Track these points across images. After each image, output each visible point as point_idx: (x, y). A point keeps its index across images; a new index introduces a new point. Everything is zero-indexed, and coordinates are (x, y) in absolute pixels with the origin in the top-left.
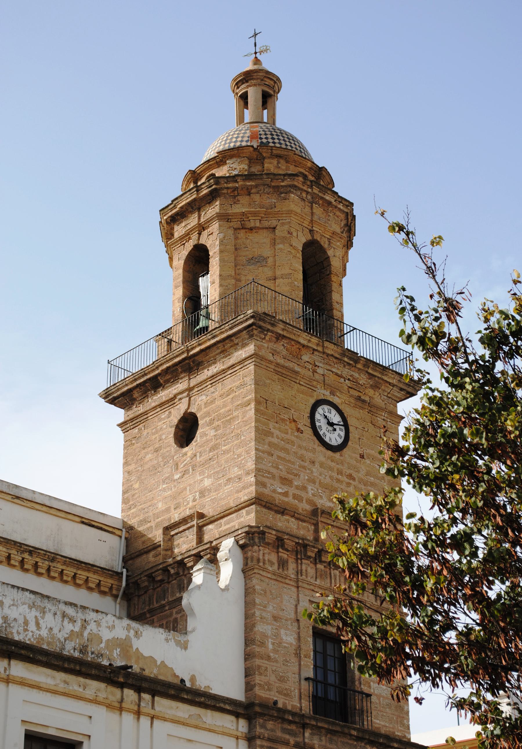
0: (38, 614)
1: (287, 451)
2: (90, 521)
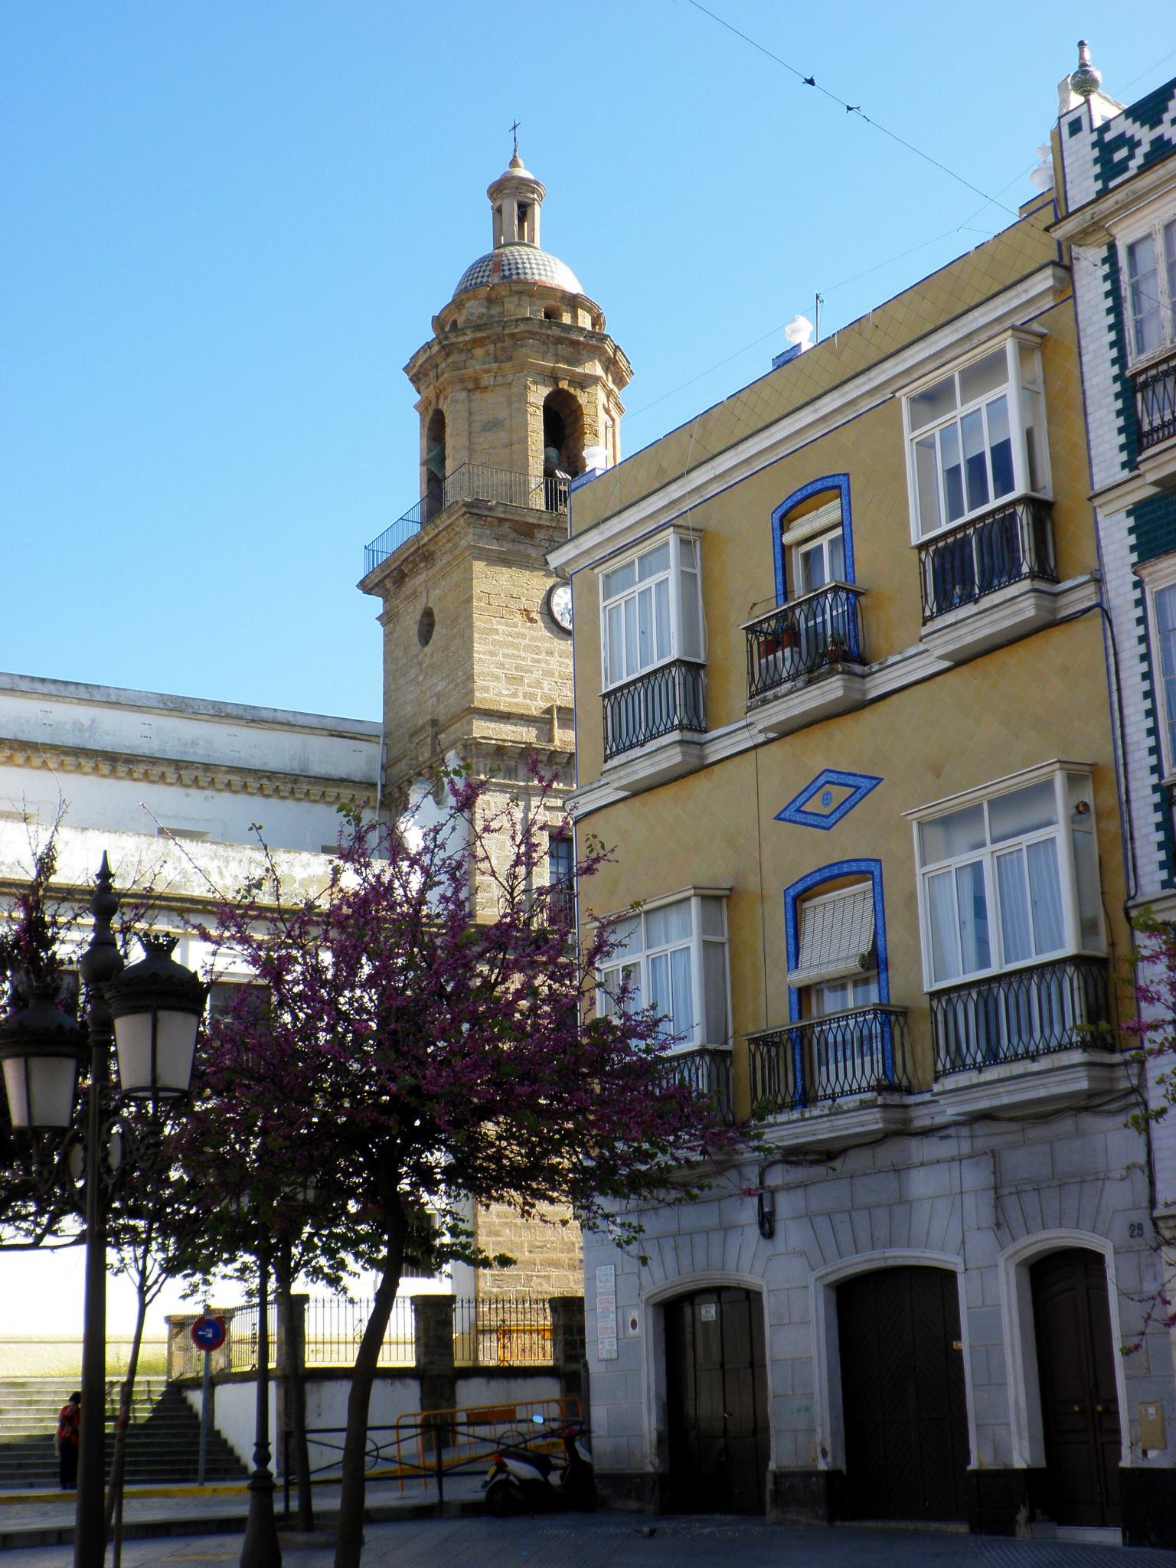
0: (221, 864)
1: (516, 646)
2: (340, 731)
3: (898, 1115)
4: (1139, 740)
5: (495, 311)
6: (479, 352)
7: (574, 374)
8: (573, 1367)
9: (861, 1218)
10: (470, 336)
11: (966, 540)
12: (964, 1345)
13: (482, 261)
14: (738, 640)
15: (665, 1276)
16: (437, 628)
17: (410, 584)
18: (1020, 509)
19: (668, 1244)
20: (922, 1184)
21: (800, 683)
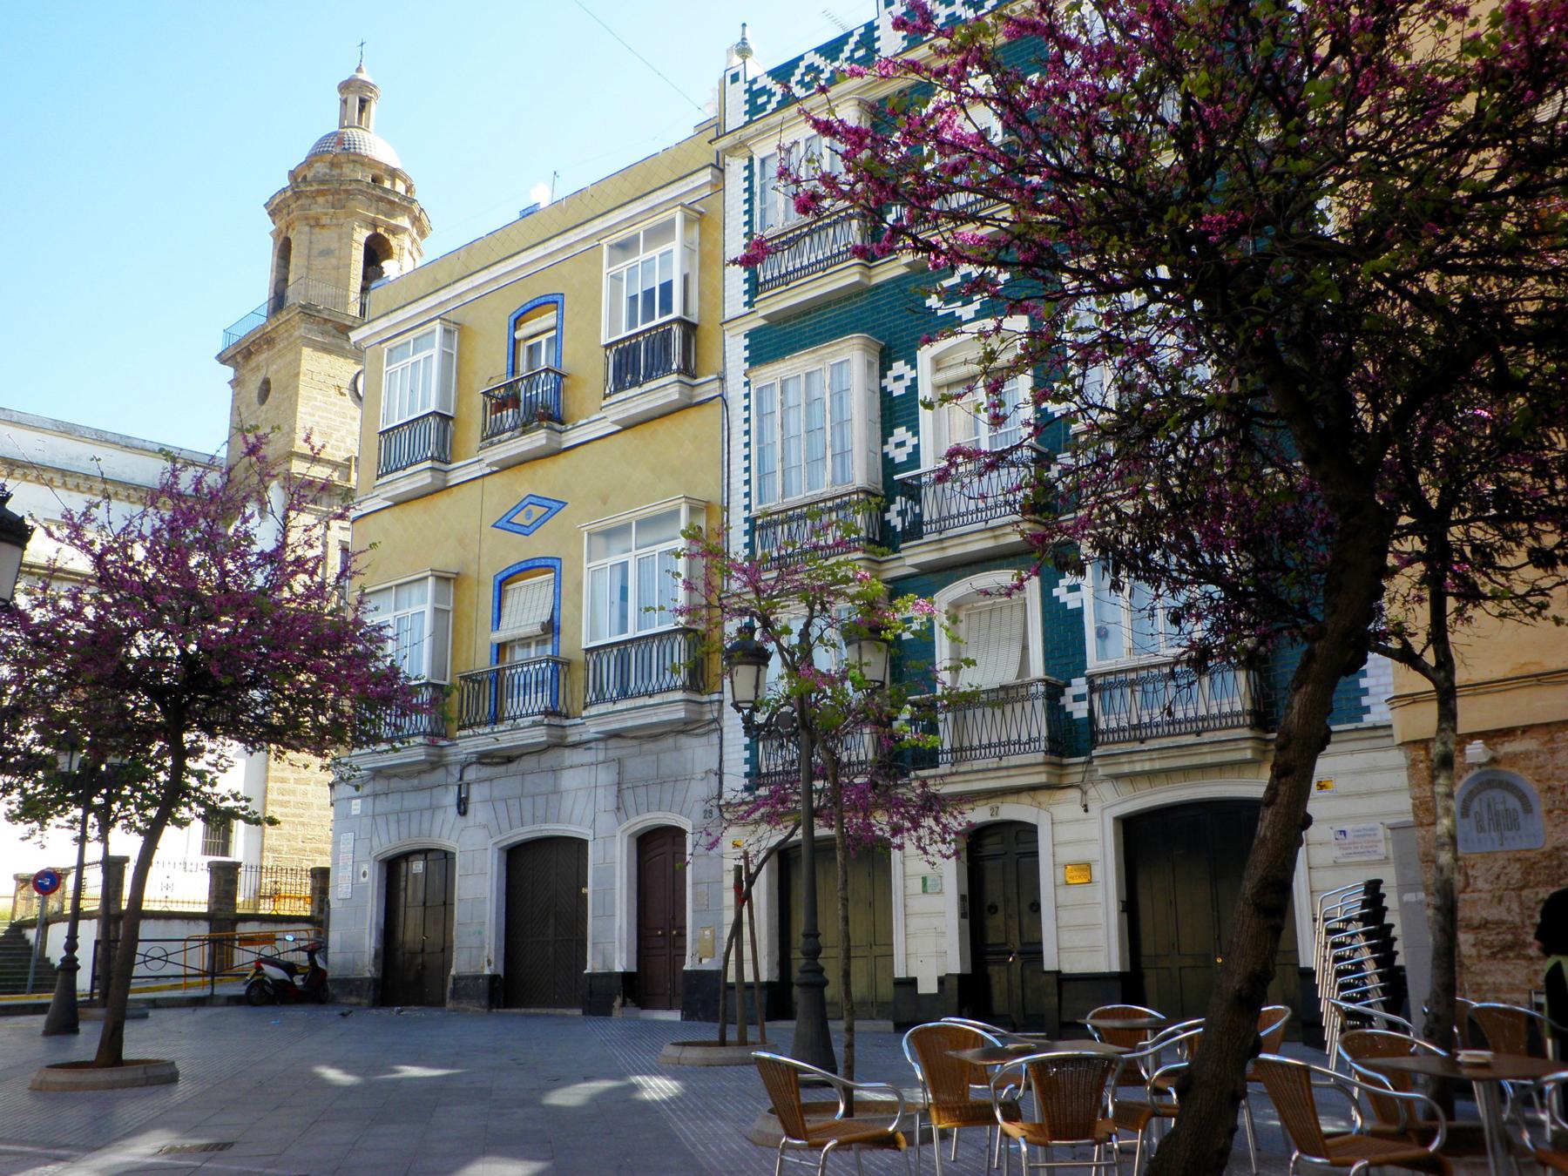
3: (557, 732)
4: (738, 488)
5: (336, 172)
6: (321, 200)
7: (389, 224)
8: (323, 917)
9: (527, 803)
10: (315, 187)
11: (638, 344)
12: (589, 890)
13: (329, 135)
14: (478, 400)
15: (389, 842)
16: (272, 393)
17: (255, 360)
18: (675, 326)
19: (393, 818)
20: (569, 780)
21: (516, 433)
